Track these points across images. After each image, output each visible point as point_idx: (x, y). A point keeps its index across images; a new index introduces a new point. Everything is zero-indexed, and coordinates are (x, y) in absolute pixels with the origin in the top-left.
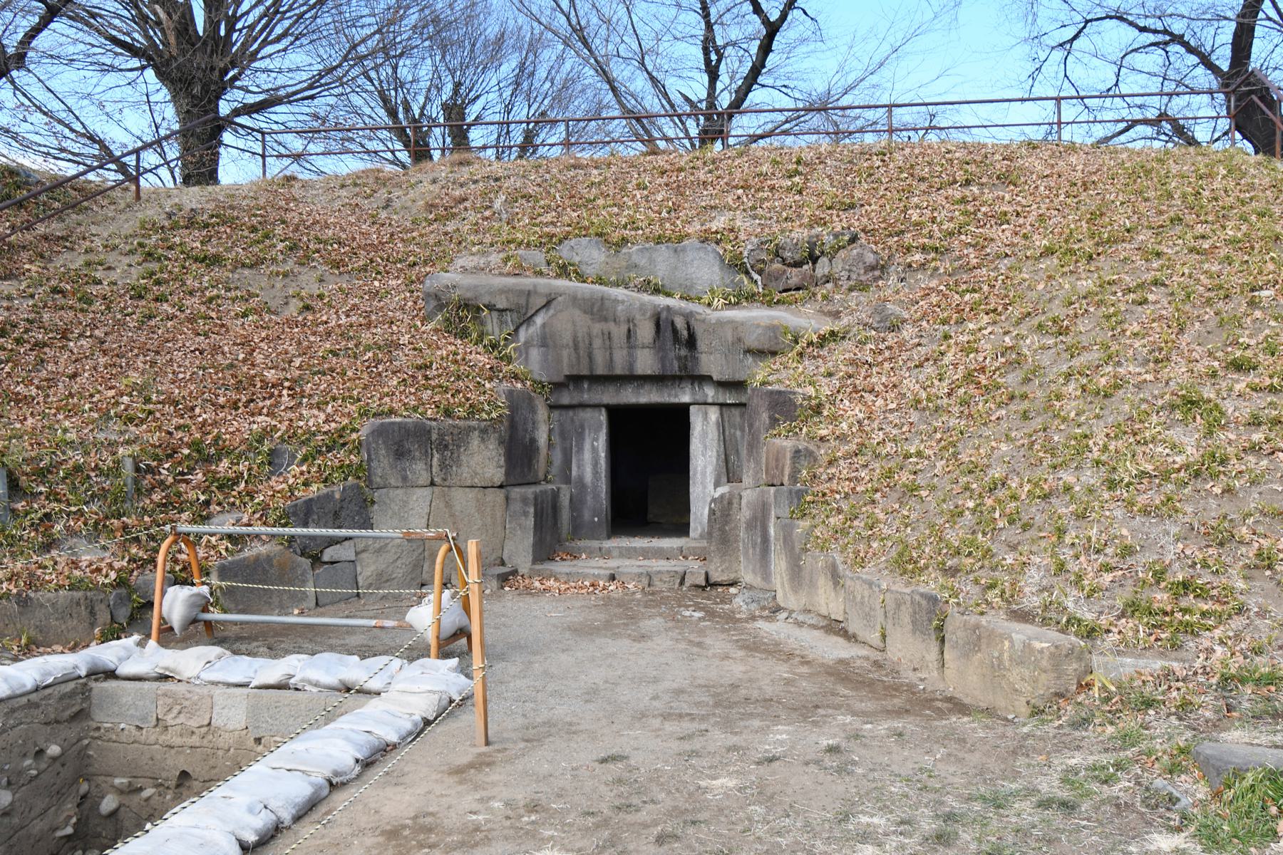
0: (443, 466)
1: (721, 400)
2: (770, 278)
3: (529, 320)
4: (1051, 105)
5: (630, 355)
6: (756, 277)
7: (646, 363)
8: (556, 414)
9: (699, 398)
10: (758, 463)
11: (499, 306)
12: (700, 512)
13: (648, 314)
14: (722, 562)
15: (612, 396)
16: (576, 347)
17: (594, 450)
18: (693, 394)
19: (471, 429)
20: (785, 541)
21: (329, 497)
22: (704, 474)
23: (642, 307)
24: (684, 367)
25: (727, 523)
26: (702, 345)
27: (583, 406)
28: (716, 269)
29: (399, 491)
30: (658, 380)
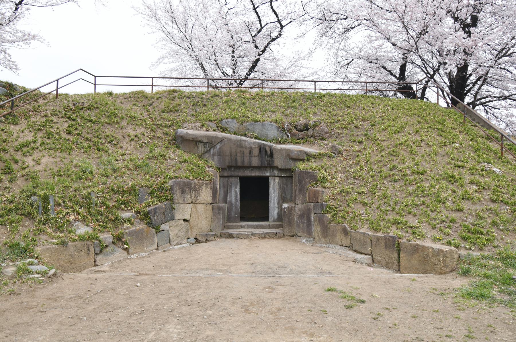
0: (196, 196)
1: (280, 175)
2: (293, 135)
3: (215, 146)
5: (250, 159)
6: (288, 134)
7: (255, 162)
8: (222, 179)
9: (272, 174)
10: (304, 195)
11: (205, 141)
12: (274, 211)
13: (257, 146)
14: (289, 229)
15: (241, 173)
16: (231, 155)
17: (236, 192)
18: (270, 173)
19: (203, 184)
20: (319, 221)
22: (274, 200)
23: (254, 143)
25: (290, 216)
26: (275, 156)
27: (232, 176)
28: (276, 131)
29: (182, 205)
30: (259, 168)
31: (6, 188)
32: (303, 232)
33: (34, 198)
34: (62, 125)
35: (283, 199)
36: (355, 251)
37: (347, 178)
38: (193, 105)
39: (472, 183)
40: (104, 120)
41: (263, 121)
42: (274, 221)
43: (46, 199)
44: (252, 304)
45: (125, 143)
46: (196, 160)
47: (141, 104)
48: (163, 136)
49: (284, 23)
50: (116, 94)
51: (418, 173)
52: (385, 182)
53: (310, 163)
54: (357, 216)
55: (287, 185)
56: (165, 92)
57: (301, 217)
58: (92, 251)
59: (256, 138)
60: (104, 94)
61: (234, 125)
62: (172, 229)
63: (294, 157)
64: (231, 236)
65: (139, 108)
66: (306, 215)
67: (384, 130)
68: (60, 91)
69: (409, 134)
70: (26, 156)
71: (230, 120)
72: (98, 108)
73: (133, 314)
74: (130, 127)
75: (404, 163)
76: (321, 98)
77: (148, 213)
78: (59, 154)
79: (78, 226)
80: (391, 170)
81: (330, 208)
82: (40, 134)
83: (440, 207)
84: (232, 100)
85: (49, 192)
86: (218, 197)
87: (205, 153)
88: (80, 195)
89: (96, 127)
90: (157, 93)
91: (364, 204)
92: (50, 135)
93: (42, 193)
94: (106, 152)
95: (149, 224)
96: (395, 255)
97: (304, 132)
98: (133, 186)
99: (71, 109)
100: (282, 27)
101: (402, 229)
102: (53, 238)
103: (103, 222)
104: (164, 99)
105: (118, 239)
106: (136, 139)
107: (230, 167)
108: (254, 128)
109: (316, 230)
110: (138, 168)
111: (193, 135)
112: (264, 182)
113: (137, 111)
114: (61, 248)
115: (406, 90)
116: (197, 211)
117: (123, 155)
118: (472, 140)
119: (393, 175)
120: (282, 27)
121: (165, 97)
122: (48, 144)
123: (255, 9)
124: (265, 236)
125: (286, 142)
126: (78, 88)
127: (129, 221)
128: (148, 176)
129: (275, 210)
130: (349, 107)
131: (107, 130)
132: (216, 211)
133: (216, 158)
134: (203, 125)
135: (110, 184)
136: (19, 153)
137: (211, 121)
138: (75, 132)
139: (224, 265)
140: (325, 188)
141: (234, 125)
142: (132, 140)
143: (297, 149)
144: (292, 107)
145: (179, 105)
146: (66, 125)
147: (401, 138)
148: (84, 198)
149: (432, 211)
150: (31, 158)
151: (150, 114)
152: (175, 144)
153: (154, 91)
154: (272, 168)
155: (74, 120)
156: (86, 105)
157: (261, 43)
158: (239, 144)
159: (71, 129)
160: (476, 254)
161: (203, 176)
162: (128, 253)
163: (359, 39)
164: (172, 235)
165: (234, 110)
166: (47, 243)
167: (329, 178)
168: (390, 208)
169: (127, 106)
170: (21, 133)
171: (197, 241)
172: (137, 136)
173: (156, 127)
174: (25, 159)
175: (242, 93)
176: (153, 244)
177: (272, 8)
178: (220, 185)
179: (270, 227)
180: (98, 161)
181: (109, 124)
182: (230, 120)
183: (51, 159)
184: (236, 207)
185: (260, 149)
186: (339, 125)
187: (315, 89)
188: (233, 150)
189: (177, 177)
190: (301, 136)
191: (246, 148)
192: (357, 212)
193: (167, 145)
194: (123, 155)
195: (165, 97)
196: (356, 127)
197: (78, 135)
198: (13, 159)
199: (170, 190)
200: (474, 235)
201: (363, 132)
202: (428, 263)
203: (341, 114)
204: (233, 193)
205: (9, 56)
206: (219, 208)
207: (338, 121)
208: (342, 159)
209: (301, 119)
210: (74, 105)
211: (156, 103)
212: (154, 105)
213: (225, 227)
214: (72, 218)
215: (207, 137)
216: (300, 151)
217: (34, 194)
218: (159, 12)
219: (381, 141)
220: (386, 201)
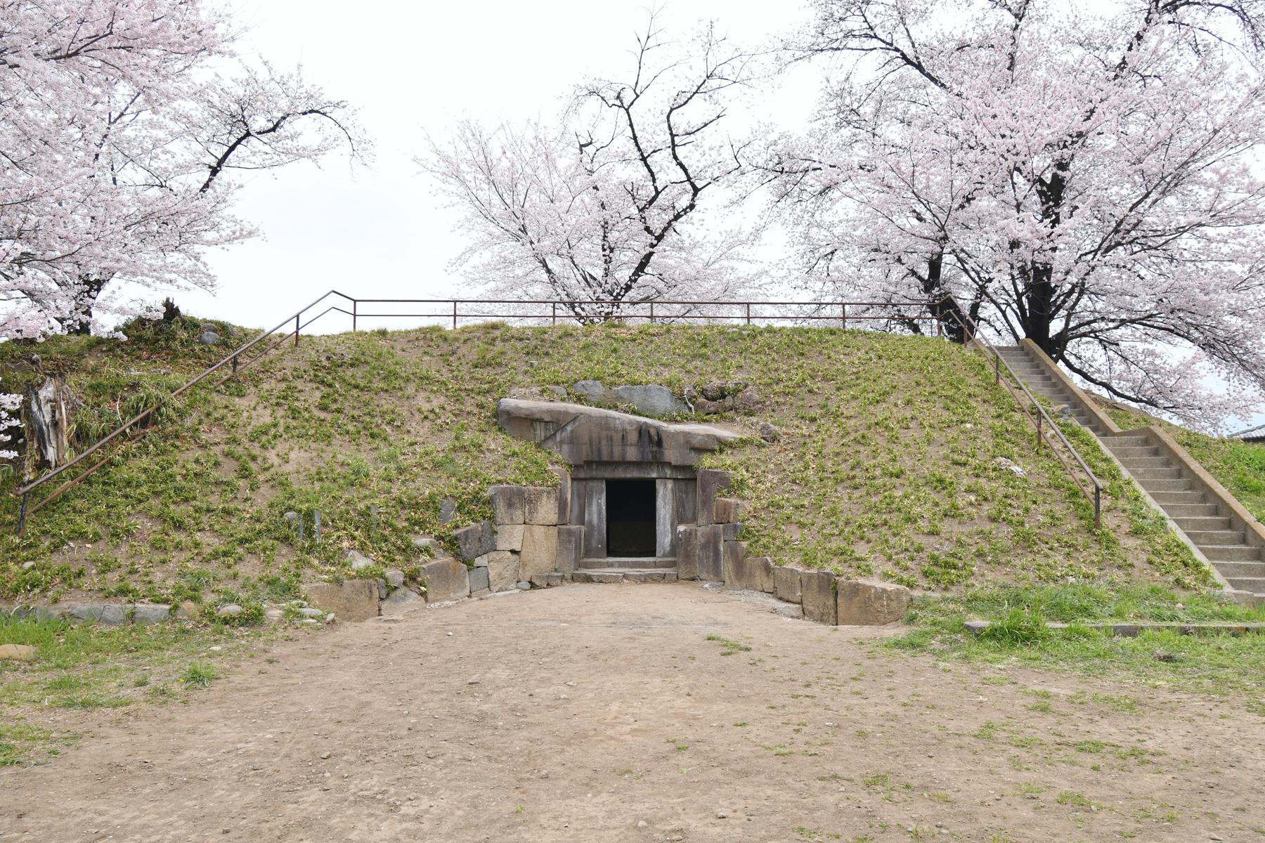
0: (530, 513)
3: (563, 428)
4: (752, 314)
7: (632, 454)
9: (662, 475)
10: (710, 512)
12: (664, 539)
17: (599, 505)
19: (543, 492)
21: (476, 529)
23: (630, 422)
24: (655, 457)
26: (665, 444)
27: (592, 479)
30: (638, 464)
31: (246, 500)
32: (708, 572)
33: (290, 514)
34: (312, 395)
35: (679, 517)
36: (781, 599)
37: (782, 481)
38: (528, 353)
39: (969, 491)
40: (378, 384)
41: (647, 383)
42: (664, 556)
43: (309, 515)
44: (602, 652)
45: (414, 424)
46: (531, 451)
47: (436, 352)
48: (476, 410)
49: (699, 184)
50: (394, 333)
51: (891, 475)
52: (839, 489)
53: (723, 456)
54: (787, 544)
55: (687, 493)
56: (478, 327)
57: (704, 546)
58: (376, 594)
59: (634, 412)
60: (373, 333)
61: (598, 390)
62: (494, 565)
63: (697, 445)
64: (588, 579)
65: (434, 360)
66: (712, 543)
67: (854, 398)
68: (302, 332)
69: (896, 405)
70: (266, 449)
71: (590, 382)
72: (366, 363)
73: (450, 660)
74: (422, 395)
75: (874, 458)
76: (755, 337)
77: (456, 538)
78: (314, 445)
79: (353, 556)
80: (853, 469)
81: (749, 532)
82: (280, 412)
83: (908, 530)
84: (595, 345)
85: (314, 506)
86: (568, 514)
87: (547, 439)
88: (355, 510)
89: (366, 397)
90: (463, 330)
91: (802, 525)
92: (295, 413)
93: (304, 507)
94: (385, 439)
95: (457, 556)
96: (831, 602)
97: (718, 402)
98: (431, 496)
99: (324, 367)
100: (696, 190)
101: (845, 562)
102: (321, 573)
103: (389, 552)
104: (477, 342)
105: (412, 578)
106: (431, 416)
107: (589, 463)
108: (631, 395)
109: (727, 567)
110: (437, 466)
111: (527, 409)
112: (647, 490)
113: (430, 366)
114: (334, 587)
115: (944, 308)
116: (532, 536)
117: (412, 444)
118: (999, 416)
119: (854, 477)
120: (696, 190)
121: (479, 338)
122: (295, 428)
123: (644, 159)
124: (645, 580)
125: (685, 419)
126: (328, 324)
127: (427, 550)
128: (454, 480)
129: (666, 536)
130: (802, 354)
131: (383, 402)
132: (565, 537)
133: (565, 447)
134: (543, 391)
135: (396, 492)
136: (256, 444)
137: (557, 383)
138: (334, 407)
139: (571, 615)
140: (743, 498)
141: (598, 390)
142: (426, 418)
143: (702, 432)
144: (701, 356)
145: (503, 353)
146: (318, 394)
147: (880, 412)
148: (361, 514)
149: (895, 535)
150: (273, 452)
151: (452, 371)
152: (495, 424)
153: (458, 326)
154: (663, 464)
155: (330, 386)
156: (347, 358)
157: (657, 220)
158: (605, 424)
159: (326, 401)
160: (937, 595)
161: (544, 479)
162: (426, 600)
163: (843, 210)
164: (492, 574)
165: (598, 363)
166: (315, 579)
167: (751, 482)
168: (836, 532)
169: (413, 356)
170: (252, 410)
171: (533, 586)
172: (432, 411)
173: (463, 394)
174: (267, 454)
175: (613, 330)
176: (463, 588)
177: (675, 158)
178: (572, 494)
179: (655, 565)
180: (375, 454)
181: (386, 391)
182: (590, 382)
183: (302, 453)
184: (600, 532)
185: (640, 433)
186: (777, 388)
187: (748, 318)
188: (595, 435)
189: (500, 482)
190: (712, 409)
191: (616, 430)
192: (787, 537)
193: (483, 427)
194: (412, 444)
195: (479, 338)
196: (810, 391)
197: (339, 411)
198: (249, 455)
199: (490, 502)
200: (943, 570)
201: (821, 400)
202: (870, 609)
203: (786, 367)
204: (594, 508)
205: (205, 264)
206: (570, 533)
207: (779, 381)
208: (778, 449)
209: (714, 379)
210: (328, 358)
211: (464, 350)
212: (460, 353)
213: (579, 566)
214: (345, 544)
215: (550, 412)
216: (708, 436)
217: (290, 509)
218: (464, 167)
219: (847, 418)
220: (833, 519)
